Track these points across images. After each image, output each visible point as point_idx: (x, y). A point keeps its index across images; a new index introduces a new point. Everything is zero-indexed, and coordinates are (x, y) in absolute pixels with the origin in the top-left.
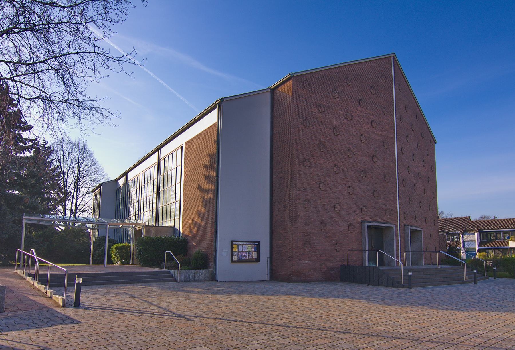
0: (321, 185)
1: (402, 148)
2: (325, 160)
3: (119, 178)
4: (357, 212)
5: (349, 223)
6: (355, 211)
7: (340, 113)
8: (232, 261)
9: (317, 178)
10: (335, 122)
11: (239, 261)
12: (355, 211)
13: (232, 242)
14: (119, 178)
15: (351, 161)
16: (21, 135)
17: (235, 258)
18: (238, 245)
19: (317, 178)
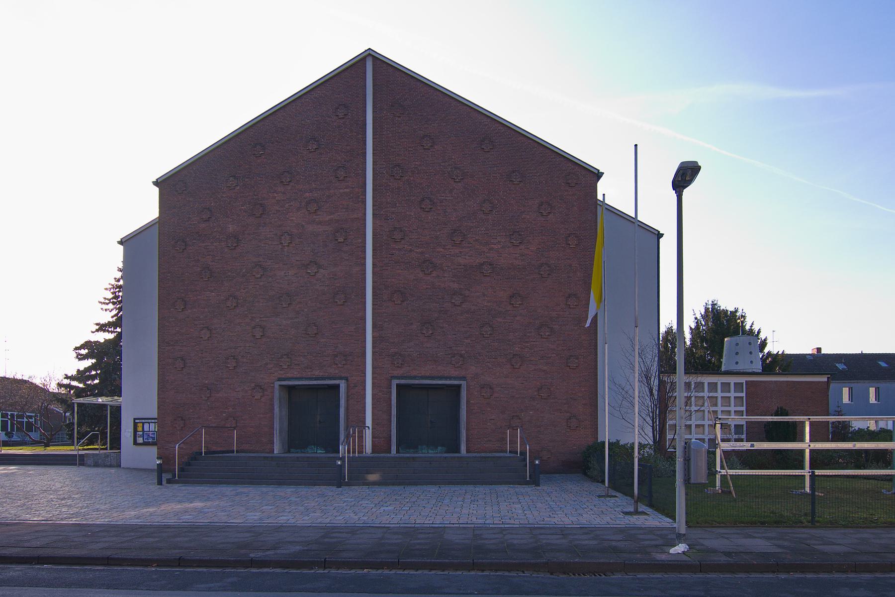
0: (202, 332)
1: (685, 175)
2: (212, 292)
3: (374, 484)
4: (269, 366)
5: (253, 385)
6: (266, 364)
7: (240, 210)
8: (135, 443)
9: (196, 322)
10: (231, 228)
11: (145, 444)
12: (266, 364)
13: (135, 419)
14: (374, 484)
15: (261, 284)
16: (769, 353)
17: (140, 440)
18: (143, 423)
19: (196, 322)
